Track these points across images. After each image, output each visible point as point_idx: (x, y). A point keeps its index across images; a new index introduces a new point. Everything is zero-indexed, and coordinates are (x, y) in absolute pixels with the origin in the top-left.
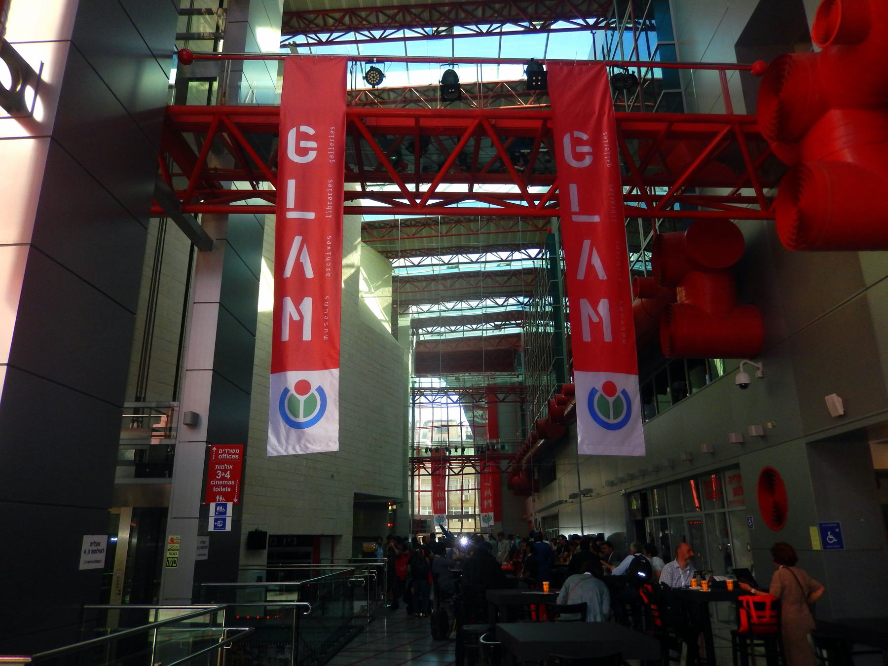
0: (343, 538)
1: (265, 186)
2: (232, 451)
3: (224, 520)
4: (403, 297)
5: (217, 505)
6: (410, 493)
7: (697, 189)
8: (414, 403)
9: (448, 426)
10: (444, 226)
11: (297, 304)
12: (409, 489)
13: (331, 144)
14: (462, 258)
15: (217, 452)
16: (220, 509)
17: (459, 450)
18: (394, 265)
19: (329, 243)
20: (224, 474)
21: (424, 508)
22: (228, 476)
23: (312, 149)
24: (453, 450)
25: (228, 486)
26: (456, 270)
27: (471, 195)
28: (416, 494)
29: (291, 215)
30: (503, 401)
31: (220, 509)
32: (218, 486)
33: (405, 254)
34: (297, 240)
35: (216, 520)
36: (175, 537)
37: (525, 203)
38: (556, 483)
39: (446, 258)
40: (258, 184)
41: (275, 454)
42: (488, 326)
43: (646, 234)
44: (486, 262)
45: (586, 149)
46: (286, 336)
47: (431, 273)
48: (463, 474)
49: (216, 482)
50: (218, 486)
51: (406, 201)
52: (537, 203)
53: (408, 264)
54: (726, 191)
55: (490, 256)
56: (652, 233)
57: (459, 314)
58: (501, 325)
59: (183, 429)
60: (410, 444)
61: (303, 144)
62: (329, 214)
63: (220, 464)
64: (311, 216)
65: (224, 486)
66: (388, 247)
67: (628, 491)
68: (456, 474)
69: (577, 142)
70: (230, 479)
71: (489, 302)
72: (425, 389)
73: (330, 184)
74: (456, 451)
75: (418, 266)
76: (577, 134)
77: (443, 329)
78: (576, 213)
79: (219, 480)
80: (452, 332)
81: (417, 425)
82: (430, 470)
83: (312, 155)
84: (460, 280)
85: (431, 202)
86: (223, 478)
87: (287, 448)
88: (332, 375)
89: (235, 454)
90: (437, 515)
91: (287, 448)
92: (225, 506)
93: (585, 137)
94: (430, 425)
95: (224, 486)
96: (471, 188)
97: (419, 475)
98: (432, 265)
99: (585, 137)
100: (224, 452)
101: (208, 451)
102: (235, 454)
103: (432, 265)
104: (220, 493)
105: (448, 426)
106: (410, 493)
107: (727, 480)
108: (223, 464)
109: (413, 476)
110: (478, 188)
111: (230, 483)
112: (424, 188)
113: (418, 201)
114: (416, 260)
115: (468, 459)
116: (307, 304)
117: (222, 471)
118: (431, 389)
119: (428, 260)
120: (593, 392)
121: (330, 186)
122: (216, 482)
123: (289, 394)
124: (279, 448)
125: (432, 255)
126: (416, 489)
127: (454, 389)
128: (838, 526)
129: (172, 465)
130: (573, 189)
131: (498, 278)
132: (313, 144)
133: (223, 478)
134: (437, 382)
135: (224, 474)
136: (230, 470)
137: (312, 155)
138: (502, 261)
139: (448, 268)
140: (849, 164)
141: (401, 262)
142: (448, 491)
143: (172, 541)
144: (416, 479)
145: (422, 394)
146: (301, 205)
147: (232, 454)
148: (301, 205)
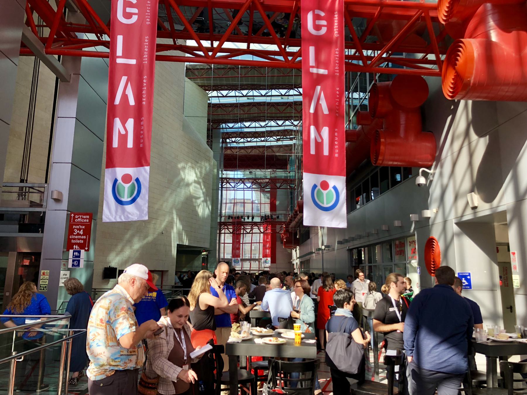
0: (169, 272)
1: (106, 38)
2: (84, 217)
3: (79, 261)
4: (216, 117)
5: (74, 252)
6: (217, 244)
7: (404, 53)
8: (222, 188)
9: (244, 203)
10: (243, 70)
11: (124, 123)
12: (218, 242)
13: (148, 11)
14: (255, 93)
15: (74, 217)
16: (76, 254)
17: (250, 218)
18: (209, 95)
19: (145, 81)
20: (79, 231)
21: (227, 254)
22: (82, 233)
23: (135, 14)
24: (246, 218)
25: (82, 239)
26: (252, 101)
27: (248, 51)
28: (222, 245)
29: (119, 61)
30: (279, 188)
31: (76, 254)
32: (74, 239)
33: (217, 88)
34: (124, 79)
35: (73, 261)
36: (46, 271)
37: (281, 58)
38: (309, 241)
39: (245, 92)
40: (101, 36)
41: (108, 221)
42: (272, 139)
43: (370, 84)
44: (271, 96)
45: (324, 23)
46: (115, 144)
47: (235, 102)
48: (252, 233)
49: (73, 237)
50: (74, 239)
51: (201, 53)
52: (290, 58)
53: (220, 95)
54: (420, 56)
55: (274, 92)
56: (373, 82)
57: (253, 130)
58: (280, 138)
59: (51, 202)
60: (219, 214)
61: (129, 10)
62: (145, 61)
63: (75, 225)
64: (133, 62)
65: (79, 239)
66: (206, 82)
67: (351, 248)
68: (248, 233)
69: (317, 17)
70: (83, 235)
71: (273, 123)
72: (230, 179)
73: (146, 40)
74: (248, 219)
75: (226, 96)
76: (317, 12)
77: (242, 140)
78: (313, 67)
79: (76, 235)
80: (248, 142)
81: (224, 201)
82: (231, 230)
83: (135, 18)
84: (254, 108)
85: (219, 54)
86: (78, 234)
87: (115, 217)
88: (145, 170)
89: (86, 219)
90: (233, 259)
91: (115, 217)
92: (79, 252)
93: (323, 14)
94: (233, 201)
95: (79, 239)
96: (248, 46)
97: (225, 233)
98: (236, 96)
99: (323, 14)
100: (79, 218)
101: (69, 217)
102: (86, 219)
103: (236, 96)
104: (76, 244)
105: (244, 203)
106: (217, 244)
107: (408, 243)
108: (78, 225)
109: (220, 233)
110: (254, 46)
111: (83, 237)
112: (216, 44)
113: (210, 54)
114: (224, 93)
115: (256, 224)
116: (130, 123)
117: (78, 229)
118: (234, 179)
119: (233, 93)
120: (315, 186)
121: (146, 41)
122: (73, 237)
123: (118, 182)
124: (110, 217)
125: (236, 90)
126: (222, 241)
127: (248, 179)
128: (469, 275)
129: (44, 225)
130: (312, 49)
131: (279, 107)
132: (135, 10)
133: (78, 234)
134: (239, 174)
135: (79, 231)
136: (83, 229)
137: (135, 18)
138: (282, 95)
139: (248, 99)
140: (361, 66)
141: (215, 93)
142: (243, 243)
143: (44, 274)
144: (222, 235)
145: (227, 182)
146: (126, 55)
147: (84, 219)
148: (126, 55)
